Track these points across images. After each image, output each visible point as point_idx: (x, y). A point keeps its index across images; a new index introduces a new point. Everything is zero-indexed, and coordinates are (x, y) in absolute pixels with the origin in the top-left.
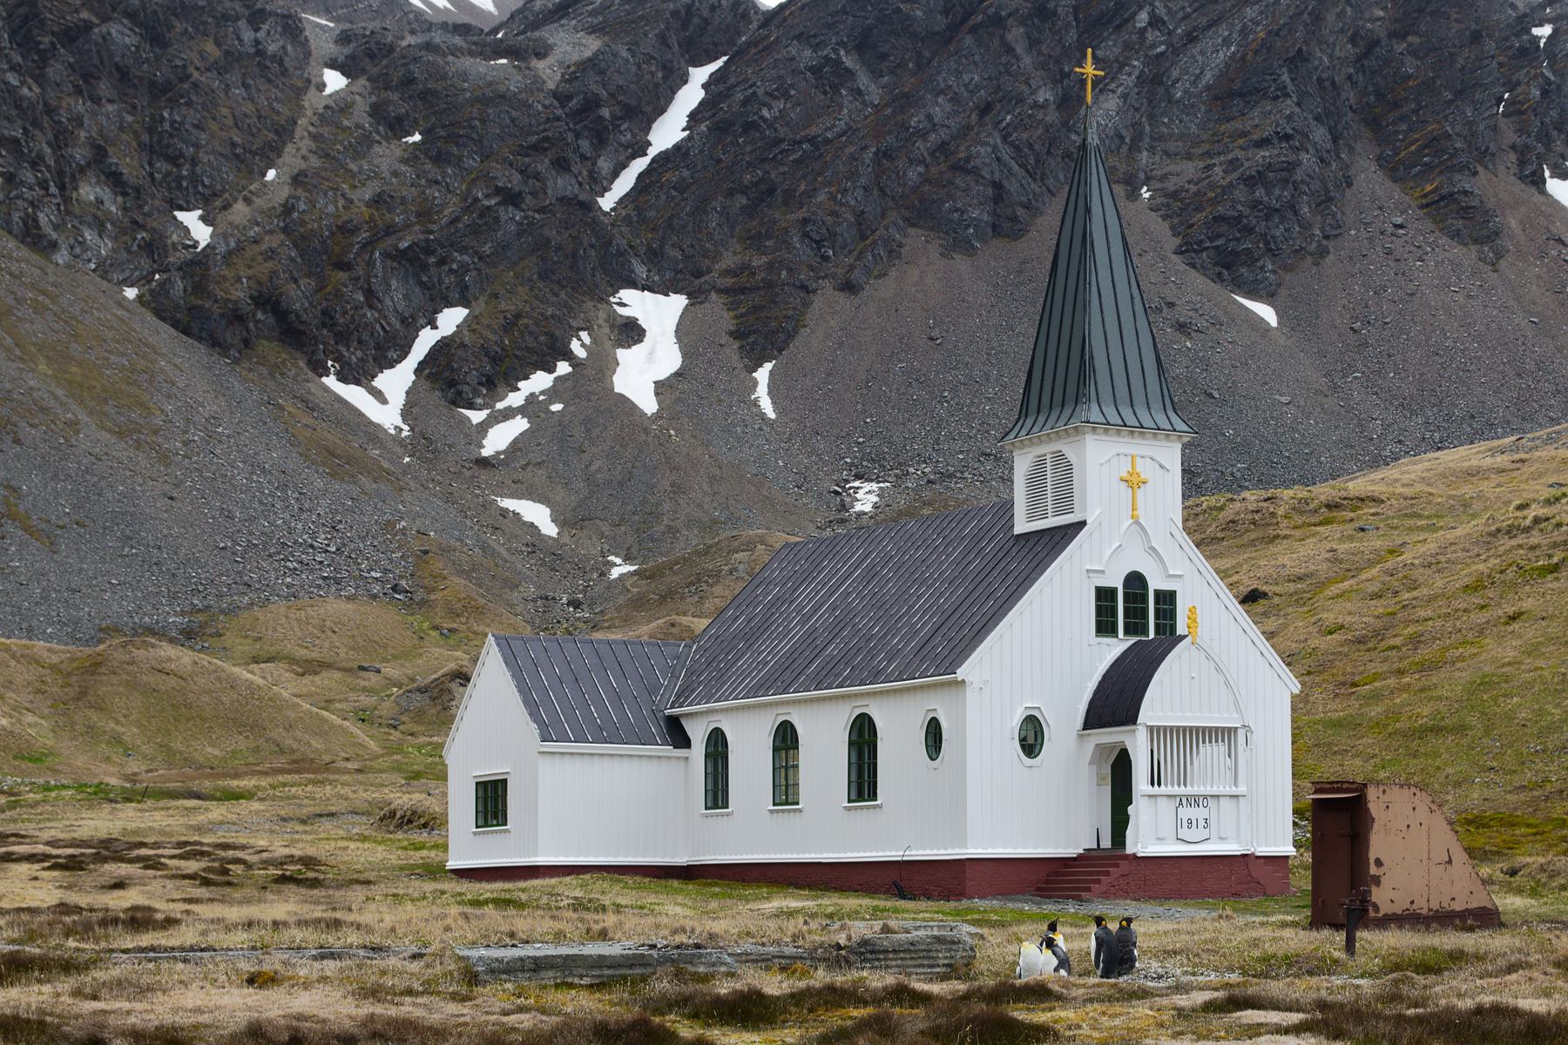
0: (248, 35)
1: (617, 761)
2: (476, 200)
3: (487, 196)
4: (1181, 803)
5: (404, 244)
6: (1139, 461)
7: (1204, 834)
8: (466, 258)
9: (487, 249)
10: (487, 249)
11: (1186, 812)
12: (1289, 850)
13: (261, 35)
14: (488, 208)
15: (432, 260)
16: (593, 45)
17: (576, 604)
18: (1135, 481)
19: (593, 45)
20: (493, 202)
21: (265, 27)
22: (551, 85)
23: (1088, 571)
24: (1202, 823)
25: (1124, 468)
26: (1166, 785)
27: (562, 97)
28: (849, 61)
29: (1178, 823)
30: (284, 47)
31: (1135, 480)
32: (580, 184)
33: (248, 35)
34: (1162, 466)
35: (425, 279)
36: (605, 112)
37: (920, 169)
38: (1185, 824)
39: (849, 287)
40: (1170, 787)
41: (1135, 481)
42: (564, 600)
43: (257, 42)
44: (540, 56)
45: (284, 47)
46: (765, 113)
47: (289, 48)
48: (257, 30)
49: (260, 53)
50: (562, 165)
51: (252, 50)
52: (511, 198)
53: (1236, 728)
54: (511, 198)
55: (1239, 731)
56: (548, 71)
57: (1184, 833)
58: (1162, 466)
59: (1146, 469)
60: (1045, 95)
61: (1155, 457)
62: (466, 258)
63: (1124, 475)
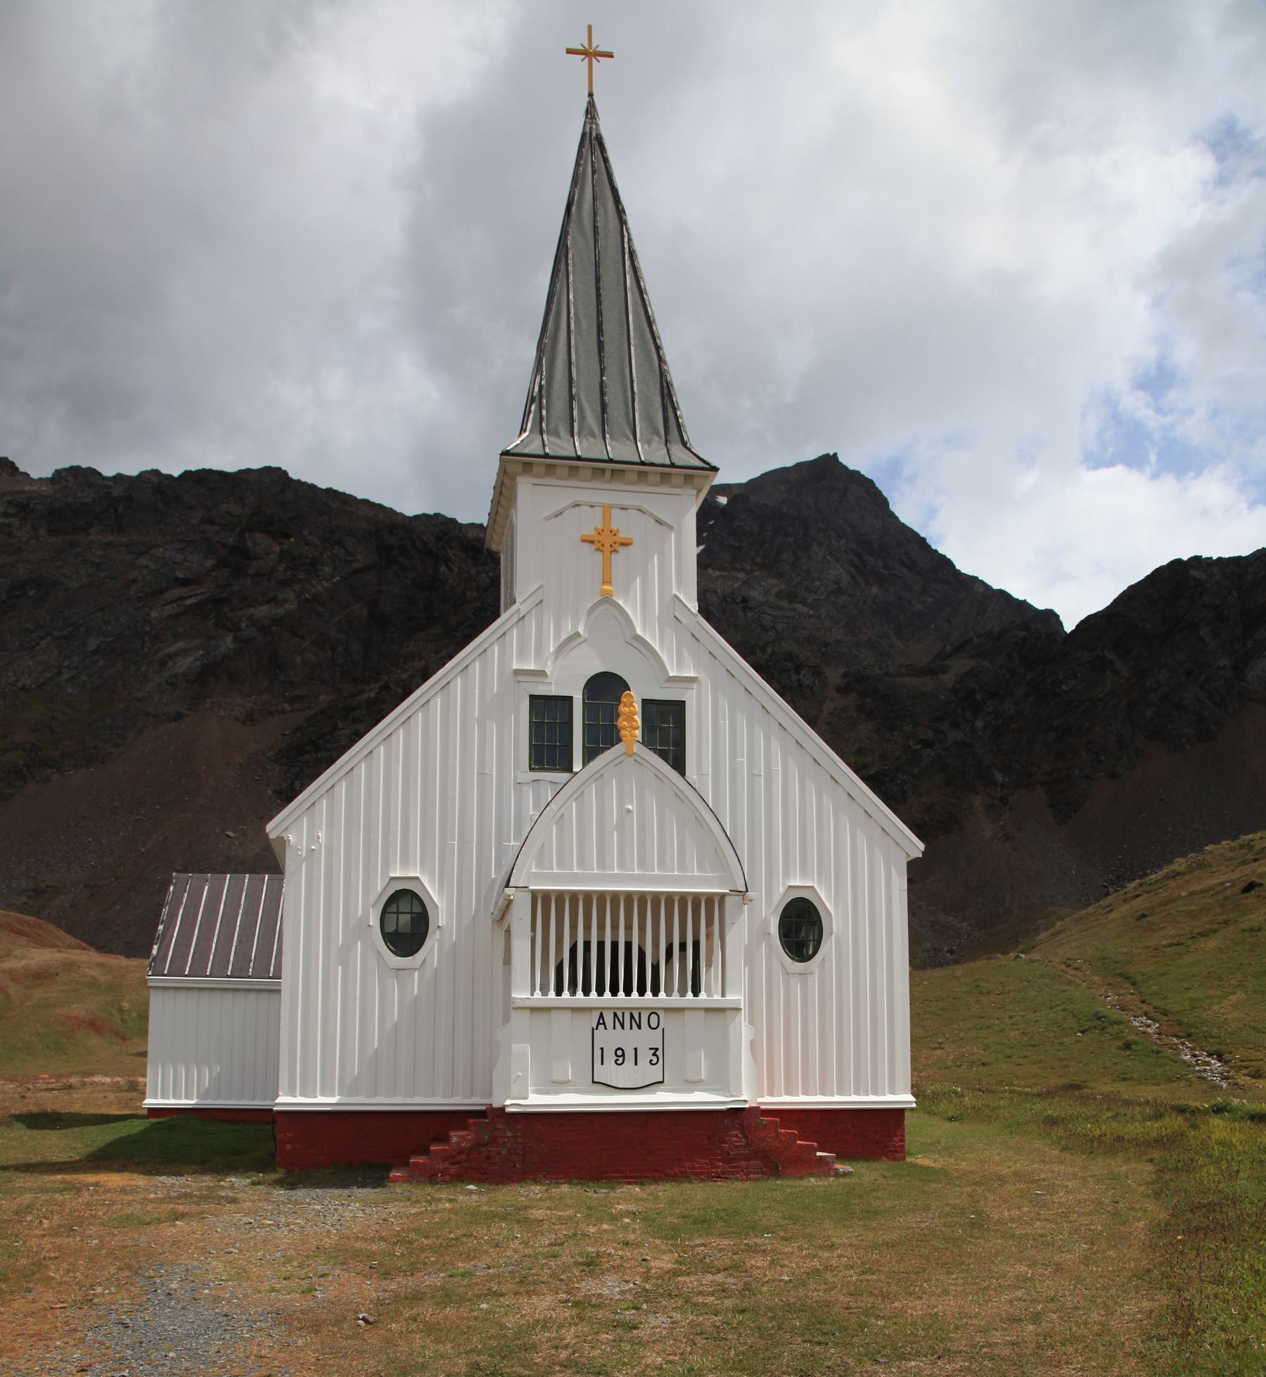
0: (794, 678)
1: (182, 996)
2: (910, 747)
3: (915, 745)
4: (601, 1021)
5: (872, 772)
6: (615, 513)
7: (655, 1074)
8: (905, 777)
9: (916, 771)
10: (916, 771)
11: (610, 1038)
12: (905, 1098)
13: (801, 676)
14: (916, 750)
15: (887, 779)
16: (971, 663)
17: (951, 952)
18: (607, 542)
19: (971, 663)
20: (918, 747)
21: (803, 672)
22: (950, 685)
23: (517, 672)
24: (646, 1056)
25: (590, 522)
26: (669, 992)
27: (954, 691)
28: (1109, 656)
29: (597, 1055)
30: (814, 682)
31: (608, 540)
32: (965, 735)
33: (794, 678)
34: (659, 522)
35: (883, 789)
36: (978, 697)
37: (1154, 709)
38: (610, 1058)
39: (1113, 776)
40: (676, 996)
41: (607, 542)
42: (946, 949)
43: (799, 680)
44: (944, 672)
45: (814, 682)
46: (1064, 687)
47: (817, 682)
48: (799, 674)
49: (800, 685)
50: (955, 725)
51: (796, 685)
52: (928, 744)
53: (722, 897)
54: (928, 744)
55: (729, 902)
56: (948, 679)
57: (609, 1071)
58: (659, 522)
59: (623, 524)
60: (1223, 662)
61: (646, 507)
62: (905, 777)
63: (589, 532)
